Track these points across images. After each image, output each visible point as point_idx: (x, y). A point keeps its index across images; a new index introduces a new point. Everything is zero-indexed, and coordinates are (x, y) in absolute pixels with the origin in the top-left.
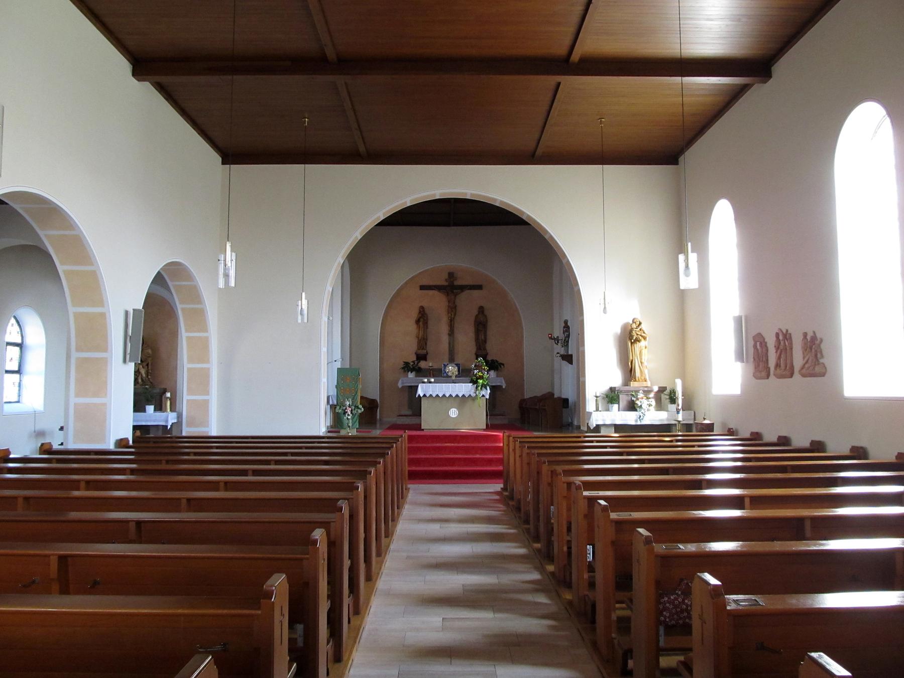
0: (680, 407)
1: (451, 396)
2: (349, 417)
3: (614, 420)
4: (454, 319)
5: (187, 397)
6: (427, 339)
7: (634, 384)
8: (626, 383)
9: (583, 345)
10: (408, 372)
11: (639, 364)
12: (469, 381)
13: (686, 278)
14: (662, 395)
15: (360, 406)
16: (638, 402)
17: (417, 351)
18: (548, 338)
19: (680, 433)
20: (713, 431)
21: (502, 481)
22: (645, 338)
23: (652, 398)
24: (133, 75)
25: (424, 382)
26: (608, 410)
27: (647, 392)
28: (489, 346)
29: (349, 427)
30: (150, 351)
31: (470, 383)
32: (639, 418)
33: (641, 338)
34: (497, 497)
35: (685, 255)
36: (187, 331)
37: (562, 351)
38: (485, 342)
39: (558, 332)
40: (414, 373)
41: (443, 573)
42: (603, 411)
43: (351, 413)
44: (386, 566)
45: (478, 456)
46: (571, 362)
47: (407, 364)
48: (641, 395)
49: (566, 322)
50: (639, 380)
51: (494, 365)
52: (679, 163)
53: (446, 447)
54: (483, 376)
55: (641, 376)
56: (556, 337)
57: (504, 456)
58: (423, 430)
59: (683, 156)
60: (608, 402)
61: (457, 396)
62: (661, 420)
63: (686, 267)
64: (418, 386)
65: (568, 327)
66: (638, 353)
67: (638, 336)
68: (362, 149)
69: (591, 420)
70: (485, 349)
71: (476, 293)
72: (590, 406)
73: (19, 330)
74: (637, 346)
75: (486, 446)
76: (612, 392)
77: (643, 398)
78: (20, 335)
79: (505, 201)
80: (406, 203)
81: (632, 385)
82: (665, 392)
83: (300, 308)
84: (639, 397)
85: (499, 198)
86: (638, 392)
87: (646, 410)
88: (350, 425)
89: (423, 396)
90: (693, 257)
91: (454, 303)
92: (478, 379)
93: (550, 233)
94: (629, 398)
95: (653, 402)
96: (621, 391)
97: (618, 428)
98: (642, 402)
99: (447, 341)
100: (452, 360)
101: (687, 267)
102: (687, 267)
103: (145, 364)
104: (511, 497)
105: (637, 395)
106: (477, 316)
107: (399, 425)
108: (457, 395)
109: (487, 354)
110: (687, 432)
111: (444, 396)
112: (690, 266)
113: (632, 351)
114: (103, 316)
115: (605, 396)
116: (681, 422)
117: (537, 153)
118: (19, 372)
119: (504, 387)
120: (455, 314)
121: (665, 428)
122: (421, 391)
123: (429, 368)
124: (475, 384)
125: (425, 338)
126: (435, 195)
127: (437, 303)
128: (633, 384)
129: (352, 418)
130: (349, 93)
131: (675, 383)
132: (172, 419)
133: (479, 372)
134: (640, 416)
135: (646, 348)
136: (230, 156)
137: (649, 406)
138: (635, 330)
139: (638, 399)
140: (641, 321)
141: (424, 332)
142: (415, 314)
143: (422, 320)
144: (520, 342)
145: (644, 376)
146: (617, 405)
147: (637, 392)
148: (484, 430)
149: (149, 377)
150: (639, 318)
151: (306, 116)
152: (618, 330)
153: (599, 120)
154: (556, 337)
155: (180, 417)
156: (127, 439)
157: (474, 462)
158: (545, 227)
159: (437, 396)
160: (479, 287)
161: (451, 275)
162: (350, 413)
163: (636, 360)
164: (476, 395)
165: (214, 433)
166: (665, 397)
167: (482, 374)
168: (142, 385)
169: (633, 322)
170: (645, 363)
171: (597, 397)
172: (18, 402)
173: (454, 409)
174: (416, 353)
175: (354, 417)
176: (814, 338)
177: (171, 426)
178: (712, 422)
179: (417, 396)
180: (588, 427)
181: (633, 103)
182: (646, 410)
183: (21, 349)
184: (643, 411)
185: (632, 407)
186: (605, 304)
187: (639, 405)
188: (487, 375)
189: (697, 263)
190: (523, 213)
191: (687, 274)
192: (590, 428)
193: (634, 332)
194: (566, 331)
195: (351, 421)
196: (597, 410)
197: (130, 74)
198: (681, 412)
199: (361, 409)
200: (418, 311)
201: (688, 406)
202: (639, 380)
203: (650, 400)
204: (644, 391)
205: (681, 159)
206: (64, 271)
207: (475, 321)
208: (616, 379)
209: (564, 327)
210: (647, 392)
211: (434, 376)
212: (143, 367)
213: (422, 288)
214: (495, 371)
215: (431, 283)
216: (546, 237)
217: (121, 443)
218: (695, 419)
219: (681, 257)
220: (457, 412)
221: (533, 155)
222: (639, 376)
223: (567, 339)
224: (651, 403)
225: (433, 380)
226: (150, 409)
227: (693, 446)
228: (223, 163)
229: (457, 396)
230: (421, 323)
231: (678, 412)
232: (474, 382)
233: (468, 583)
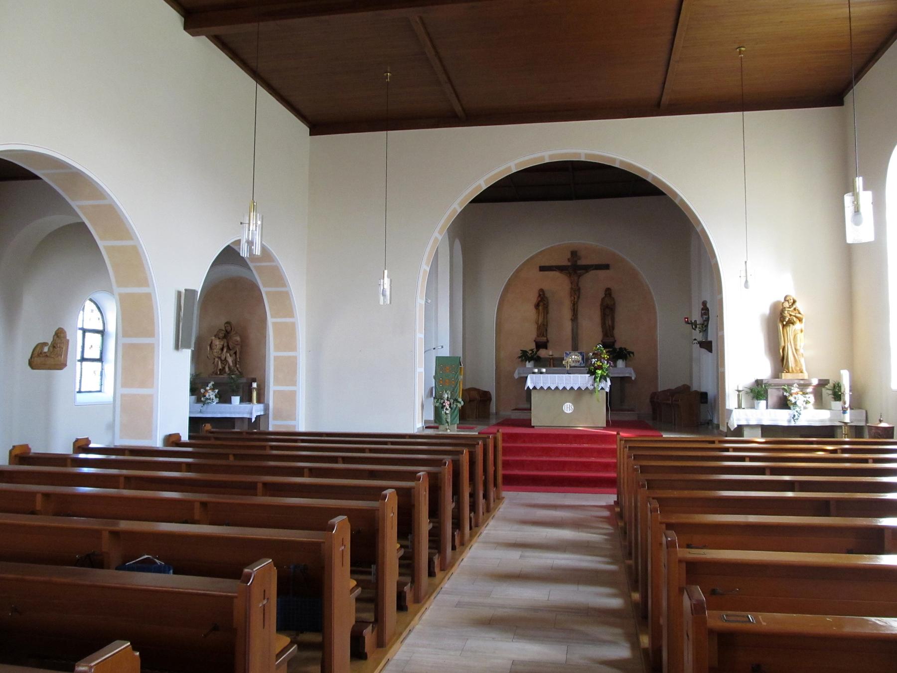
0: (847, 405)
1: (564, 388)
2: (447, 412)
3: (761, 420)
4: (577, 303)
5: (273, 388)
6: (547, 325)
7: (786, 377)
8: (777, 375)
9: (722, 329)
10: (526, 361)
11: (793, 352)
12: (586, 372)
13: (854, 226)
14: (824, 390)
15: (460, 400)
16: (791, 398)
17: (536, 338)
18: (684, 323)
19: (847, 440)
20: (892, 437)
21: (615, 490)
22: (800, 320)
23: (811, 393)
24: (185, 29)
25: (534, 373)
26: (753, 407)
27: (803, 386)
28: (617, 332)
29: (447, 422)
30: (238, 339)
31: (588, 373)
32: (793, 418)
33: (795, 319)
34: (606, 513)
35: (853, 195)
36: (272, 317)
39: (696, 316)
40: (532, 363)
41: (493, 635)
42: (748, 408)
43: (450, 407)
44: (424, 617)
45: (593, 459)
46: (710, 351)
47: (524, 353)
48: (795, 389)
49: (704, 303)
50: (792, 370)
51: (618, 354)
52: (845, 103)
53: (557, 448)
54: (602, 366)
55: (796, 366)
56: (693, 321)
57: (617, 460)
58: (533, 427)
59: (851, 91)
60: (753, 398)
61: (572, 388)
62: (822, 421)
63: (855, 212)
64: (527, 377)
65: (708, 310)
66: (792, 338)
67: (792, 317)
68: (458, 108)
69: (732, 419)
70: (612, 336)
71: (602, 273)
72: (731, 402)
73: (100, 316)
74: (791, 329)
75: (603, 448)
76: (758, 385)
77: (798, 394)
78: (102, 322)
79: (624, 159)
80: (510, 168)
81: (783, 378)
82: (826, 386)
83: (382, 288)
84: (792, 391)
85: (618, 157)
87: (802, 409)
88: (449, 420)
89: (533, 389)
90: (866, 198)
91: (578, 285)
92: (596, 369)
93: (651, 174)
94: (781, 393)
95: (811, 398)
96: (770, 385)
97: (766, 430)
98: (797, 397)
100: (575, 348)
101: (857, 211)
102: (857, 211)
103: (232, 352)
104: (621, 516)
105: (791, 390)
106: (603, 299)
107: (513, 420)
109: (615, 341)
110: (856, 438)
111: (557, 388)
112: (862, 210)
113: (784, 336)
114: (148, 297)
115: (749, 391)
116: (849, 424)
117: (664, 99)
118: (100, 360)
119: (633, 378)
120: (579, 297)
121: (826, 432)
123: (548, 357)
124: (593, 375)
125: (545, 324)
126: (543, 158)
127: (558, 285)
128: (785, 375)
129: (452, 414)
130: (428, 34)
131: (840, 376)
132: (257, 411)
133: (597, 361)
134: (794, 416)
136: (318, 127)
137: (806, 403)
138: (787, 309)
139: (791, 395)
140: (795, 298)
141: (544, 318)
142: (533, 298)
143: (541, 304)
144: (654, 328)
146: (765, 402)
147: (791, 385)
148: (604, 428)
149: (238, 366)
150: (793, 295)
151: (389, 70)
152: (767, 311)
153: (738, 50)
154: (693, 321)
155: (266, 409)
156: (178, 436)
157: (587, 466)
158: (664, 180)
159: (549, 388)
160: (606, 267)
161: (574, 254)
162: (448, 408)
164: (594, 388)
165: (302, 428)
166: (827, 392)
167: (601, 364)
168: (229, 374)
169: (786, 299)
170: (801, 351)
171: (739, 391)
172: (100, 391)
173: (568, 404)
174: (535, 341)
175: (454, 411)
177: (256, 418)
178: (891, 426)
179: (526, 389)
180: (728, 428)
181: (781, 22)
182: (802, 409)
183: (103, 336)
184: (798, 409)
185: (784, 404)
186: (746, 276)
188: (607, 364)
189: (872, 206)
190: (647, 173)
191: (857, 221)
192: (730, 429)
193: (786, 312)
195: (449, 415)
196: (740, 407)
197: (182, 28)
198: (848, 411)
199: (460, 403)
200: (538, 295)
201: (857, 403)
202: (792, 370)
203: (807, 396)
204: (800, 385)
205: (848, 98)
206: (106, 248)
207: (602, 305)
208: (764, 370)
209: (702, 309)
210: (803, 386)
211: (544, 367)
212: (230, 355)
213: (543, 269)
214: (623, 361)
215: (554, 264)
216: (677, 202)
217: (172, 440)
218: (867, 421)
219: (848, 199)
220: (573, 407)
221: (659, 104)
222: (793, 366)
223: (706, 323)
224: (808, 400)
225: (544, 370)
226: (236, 400)
227: (866, 461)
228: (311, 134)
229: (572, 388)
230: (541, 308)
231: (844, 412)
232: (592, 373)
233: (522, 658)
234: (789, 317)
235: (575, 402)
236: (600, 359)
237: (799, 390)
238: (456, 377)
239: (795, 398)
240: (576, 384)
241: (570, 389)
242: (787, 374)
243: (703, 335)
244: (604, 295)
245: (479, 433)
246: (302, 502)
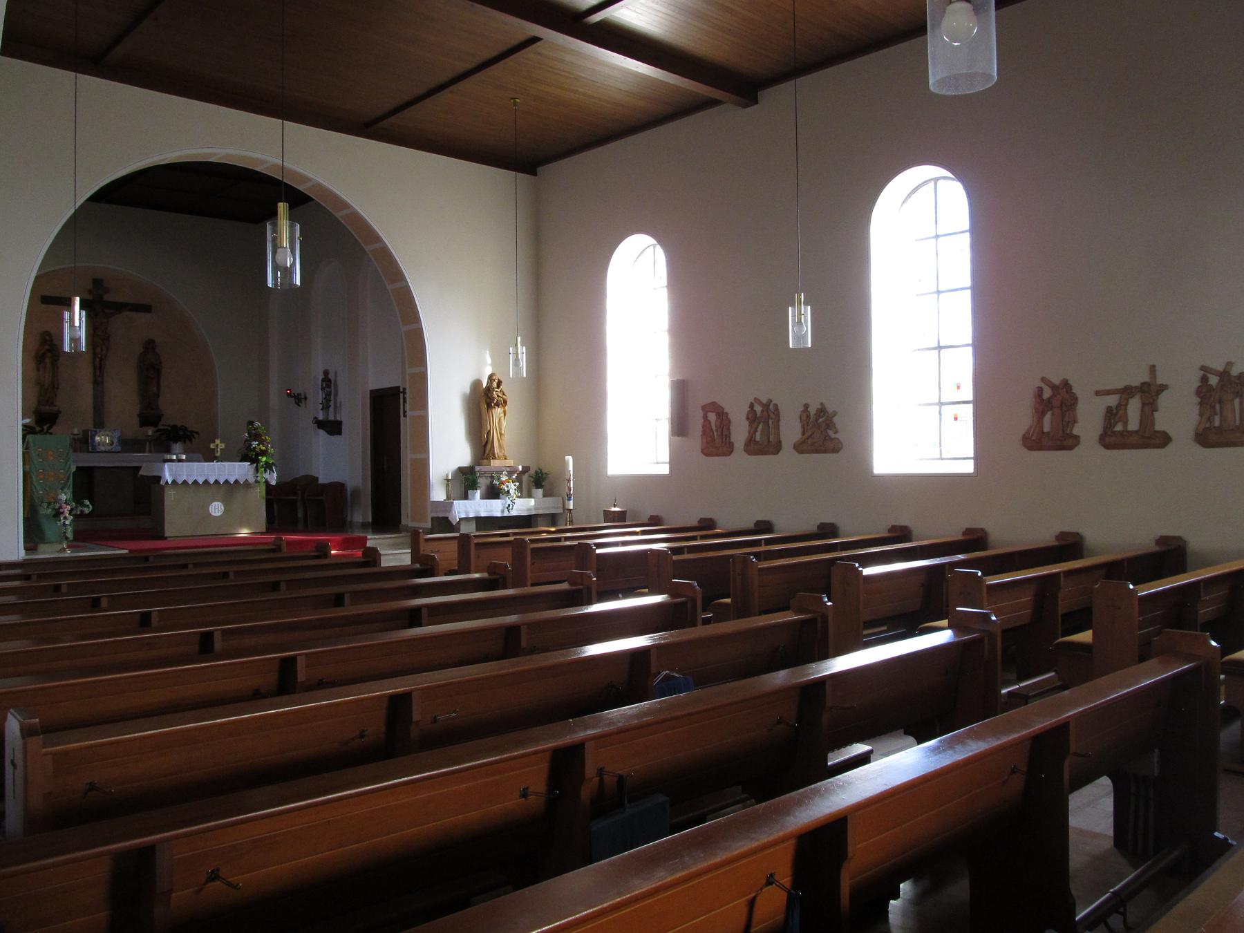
7: (495, 463)
18: (286, 396)
25: (172, 461)
38: (158, 396)
48: (504, 478)
71: (141, 318)
86: (500, 474)
92: (258, 455)
94: (488, 481)
99: (91, 392)
108: (206, 480)
111: (206, 482)
122: (170, 475)
124: (254, 463)
134: (509, 505)
139: (503, 483)
159: (196, 482)
160: (147, 309)
167: (264, 448)
173: (216, 503)
176: (822, 411)
185: (494, 492)
187: (506, 489)
199: (88, 506)
205: (540, 169)
209: (323, 380)
220: (223, 507)
225: (184, 457)
230: (48, 361)
232: (254, 461)
235: (226, 501)
236: (262, 442)
238: (67, 468)
239: (508, 487)
240: (232, 475)
241: (183, 483)
244: (1200, 418)
245: (130, 551)
246: (467, 627)
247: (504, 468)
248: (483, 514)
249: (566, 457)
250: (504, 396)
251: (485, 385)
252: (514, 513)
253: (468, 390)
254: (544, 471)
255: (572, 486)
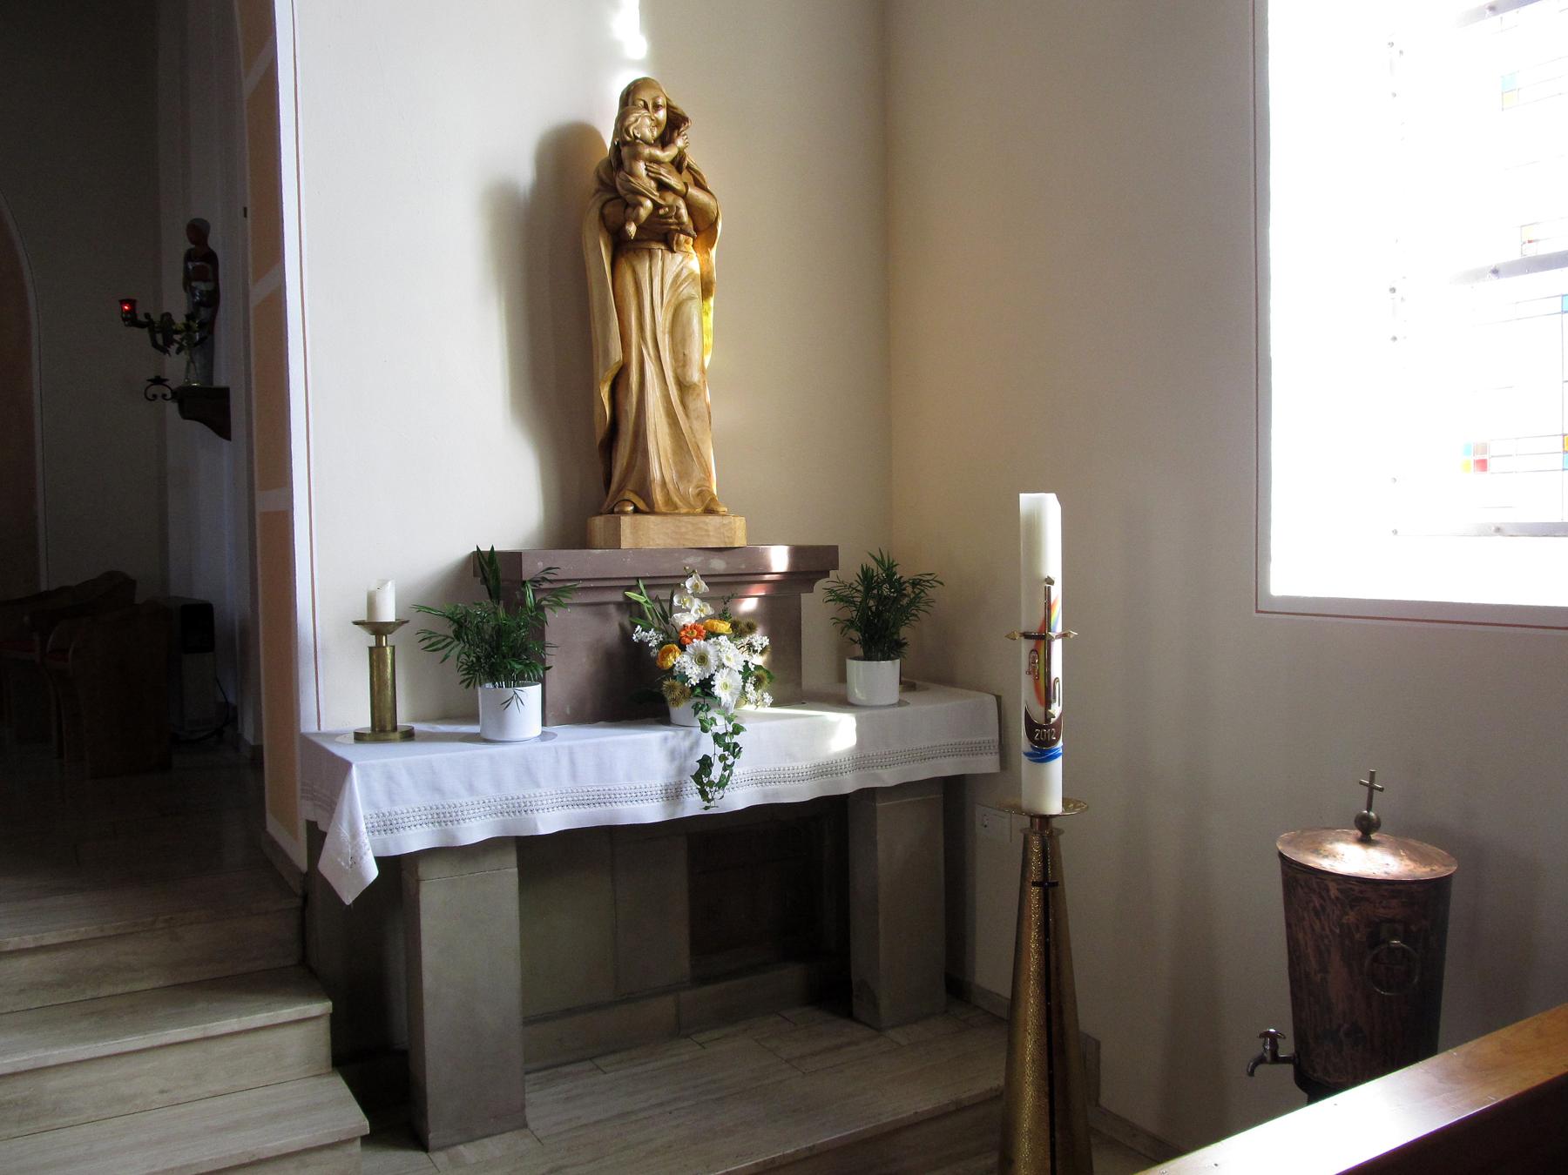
3: (521, 808)
22: (704, 227)
32: (697, 778)
37: (176, 367)
39: (177, 305)
46: (223, 429)
48: (690, 612)
49: (198, 231)
50: (668, 500)
55: (684, 474)
65: (211, 258)
66: (663, 319)
81: (626, 543)
94: (610, 630)
128: (635, 528)
134: (706, 763)
135: (706, 290)
138: (647, 151)
140: (683, 107)
145: (697, 474)
147: (673, 583)
163: (650, 369)
171: (378, 629)
193: (641, 167)
194: (200, 275)
196: (383, 729)
204: (713, 579)
209: (189, 257)
222: (671, 475)
223: (204, 313)
234: (656, 195)
237: (709, 610)
239: (702, 659)
242: (639, 517)
243: (191, 361)
247: (692, 560)
248: (549, 822)
249: (1025, 499)
250: (694, 192)
251: (608, 139)
252: (738, 797)
253: (523, 172)
254: (902, 572)
255: (1057, 670)
